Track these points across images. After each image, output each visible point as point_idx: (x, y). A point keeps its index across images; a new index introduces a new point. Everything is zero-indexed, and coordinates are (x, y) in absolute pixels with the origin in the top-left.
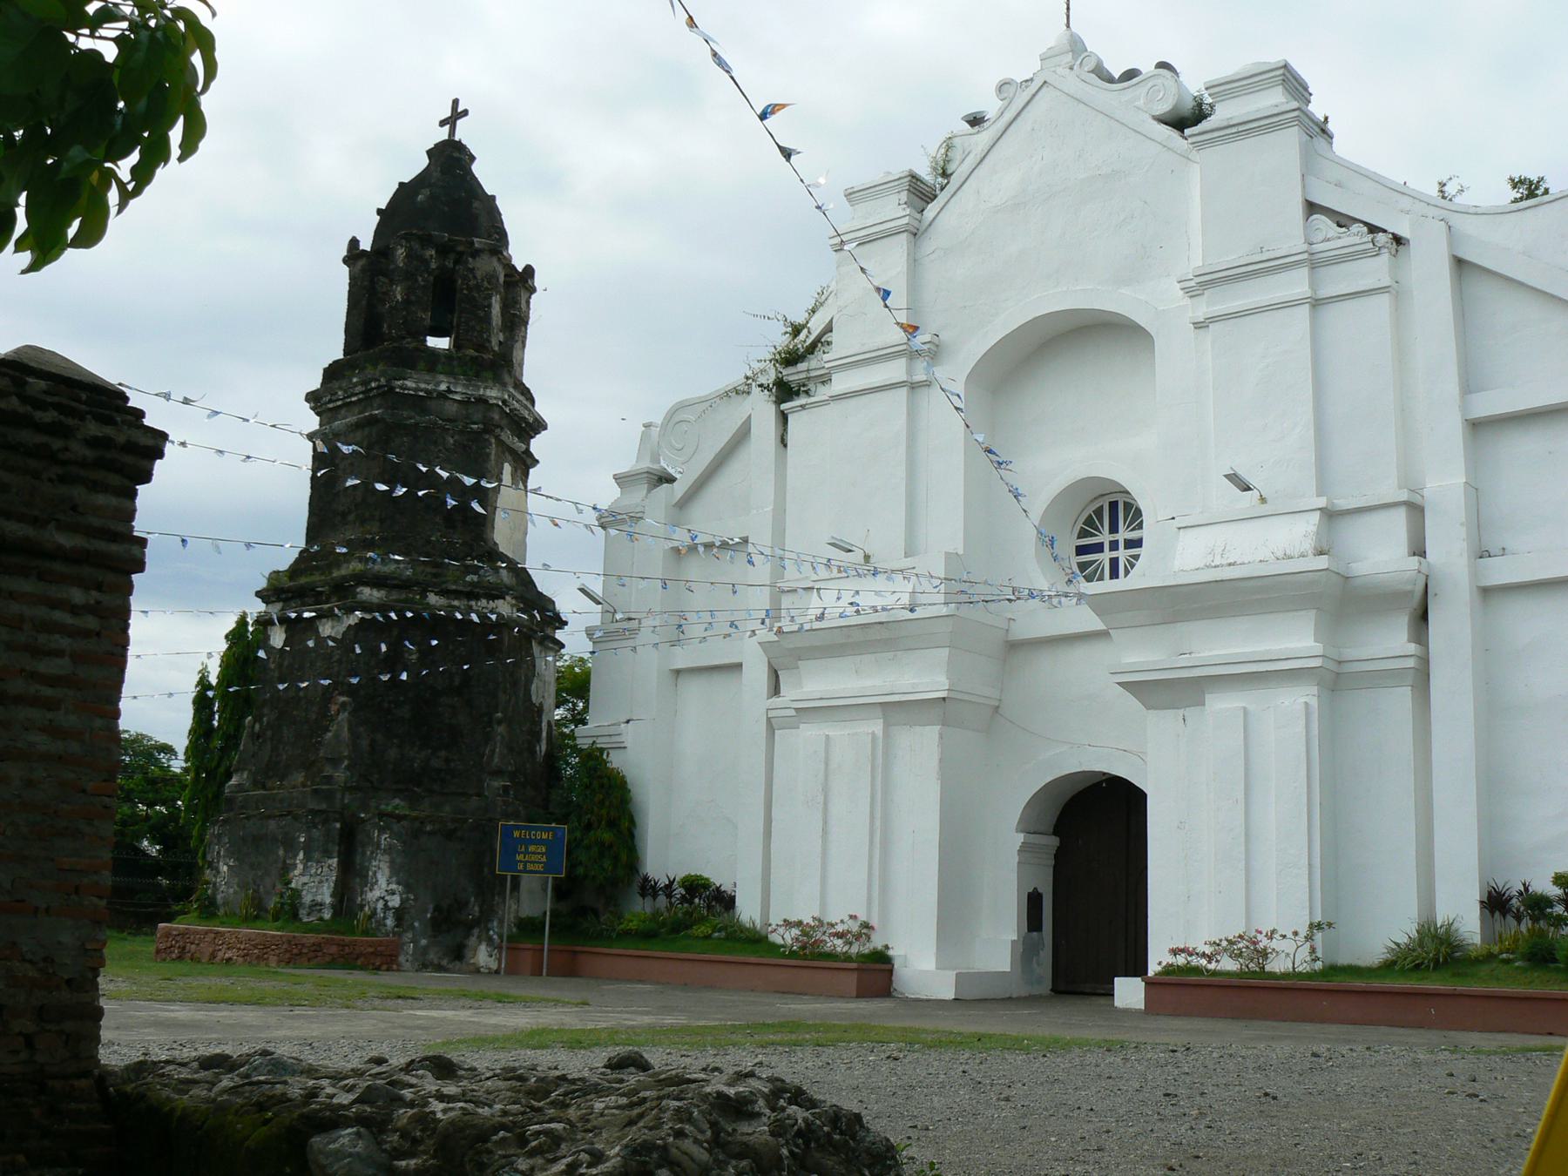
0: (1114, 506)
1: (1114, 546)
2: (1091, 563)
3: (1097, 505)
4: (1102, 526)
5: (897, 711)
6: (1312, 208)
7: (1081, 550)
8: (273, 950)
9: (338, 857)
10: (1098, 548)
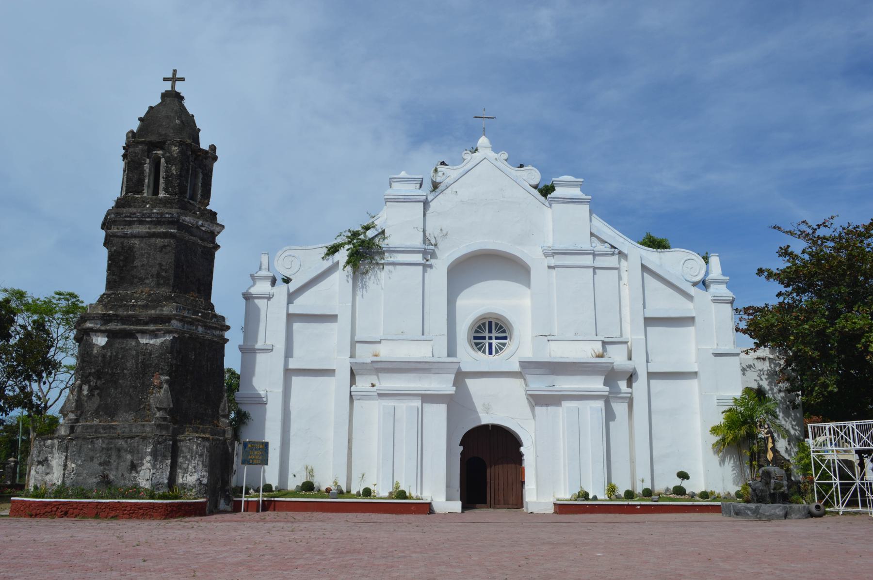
0: (490, 323)
1: (490, 338)
4: (485, 330)
5: (428, 398)
6: (592, 234)
7: (490, 353)
9: (171, 459)
10: (484, 338)
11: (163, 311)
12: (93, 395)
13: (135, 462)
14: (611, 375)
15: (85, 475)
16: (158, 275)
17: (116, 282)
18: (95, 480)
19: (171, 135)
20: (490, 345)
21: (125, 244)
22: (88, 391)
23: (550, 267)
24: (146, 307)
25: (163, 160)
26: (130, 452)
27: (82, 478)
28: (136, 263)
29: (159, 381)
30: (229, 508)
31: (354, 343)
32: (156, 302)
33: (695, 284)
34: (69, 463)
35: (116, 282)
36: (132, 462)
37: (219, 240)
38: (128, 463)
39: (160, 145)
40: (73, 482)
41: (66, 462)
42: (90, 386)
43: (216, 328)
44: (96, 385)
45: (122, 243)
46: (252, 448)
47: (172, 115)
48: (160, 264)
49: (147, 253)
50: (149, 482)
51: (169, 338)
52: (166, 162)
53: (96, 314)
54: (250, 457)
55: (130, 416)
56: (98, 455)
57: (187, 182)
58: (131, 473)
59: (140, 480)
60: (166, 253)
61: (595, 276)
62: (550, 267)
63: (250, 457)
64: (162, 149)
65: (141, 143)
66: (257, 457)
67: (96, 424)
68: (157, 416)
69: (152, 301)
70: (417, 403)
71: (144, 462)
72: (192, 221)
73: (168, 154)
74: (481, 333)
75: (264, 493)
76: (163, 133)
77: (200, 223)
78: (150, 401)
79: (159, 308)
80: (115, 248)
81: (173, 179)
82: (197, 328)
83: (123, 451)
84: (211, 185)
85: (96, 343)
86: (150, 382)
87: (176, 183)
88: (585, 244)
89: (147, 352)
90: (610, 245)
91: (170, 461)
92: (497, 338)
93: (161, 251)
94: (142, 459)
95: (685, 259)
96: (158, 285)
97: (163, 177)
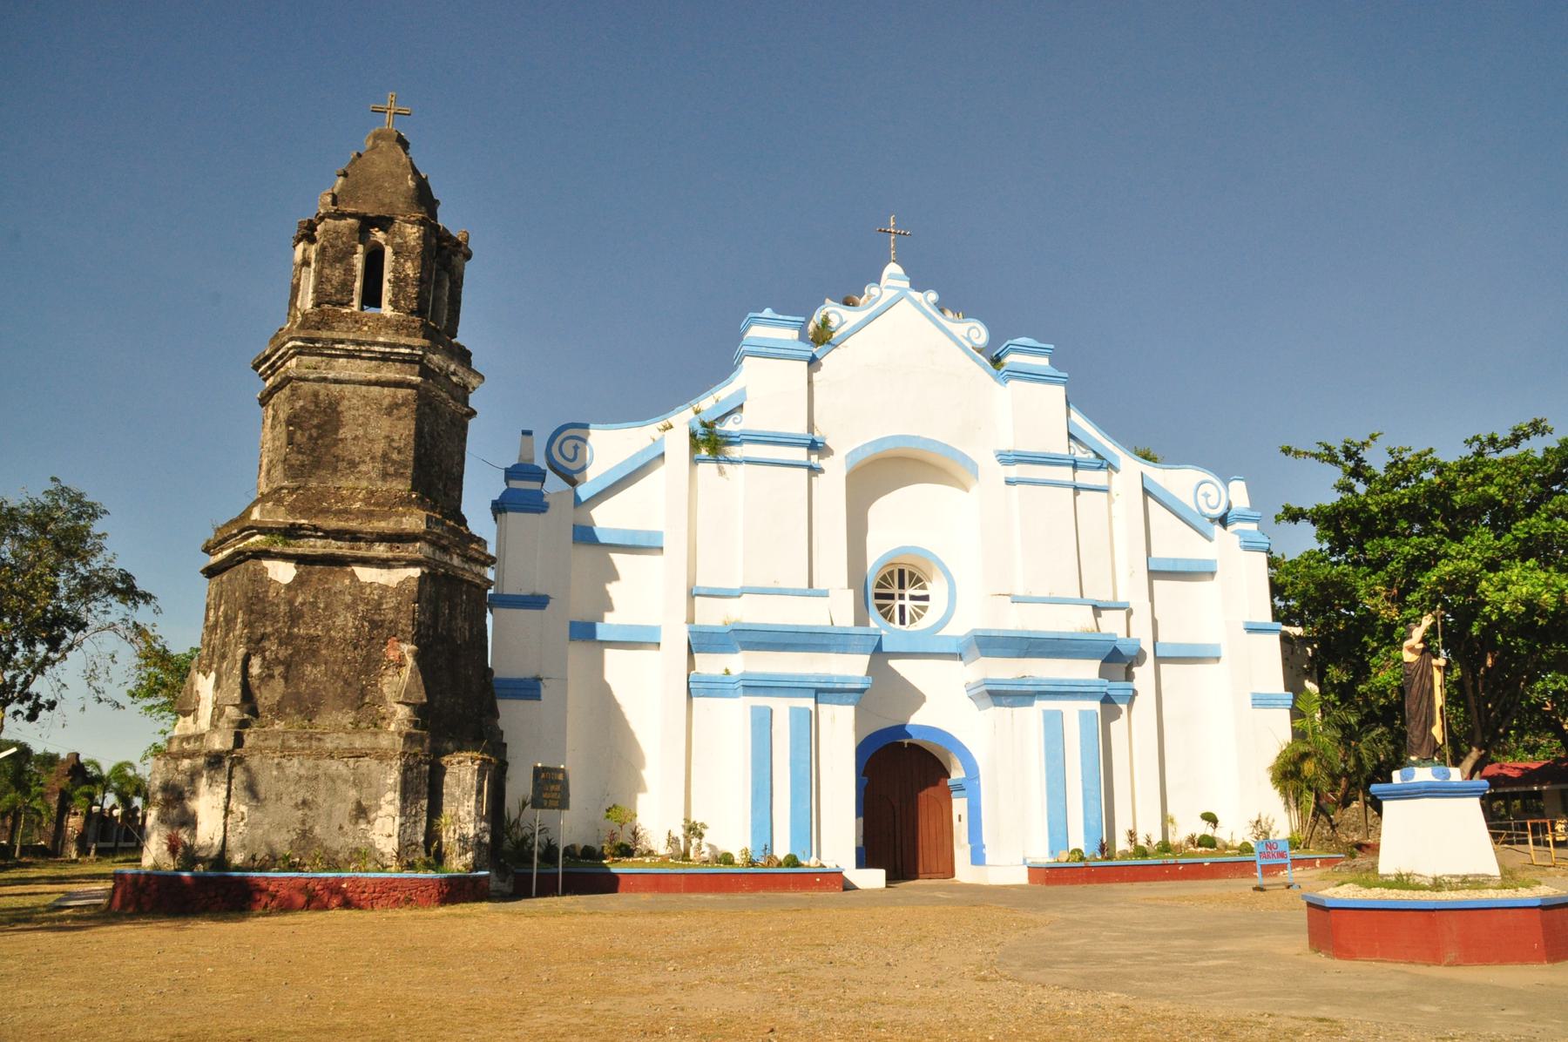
0: (901, 572)
2: (887, 605)
3: (890, 569)
5: (824, 692)
8: (422, 892)
10: (891, 597)
11: (401, 522)
12: (271, 676)
13: (364, 803)
14: (1119, 661)
15: (267, 827)
16: (385, 457)
17: (303, 466)
18: (287, 837)
19: (400, 206)
20: (902, 608)
21: (321, 398)
22: (260, 667)
23: (1008, 482)
24: (370, 515)
25: (388, 251)
26: (355, 784)
27: (260, 832)
28: (342, 433)
29: (398, 653)
30: (507, 888)
31: (692, 595)
32: (388, 505)
33: (1213, 520)
34: (233, 804)
35: (303, 466)
36: (359, 803)
37: (474, 401)
38: (351, 806)
39: (385, 223)
40: (243, 840)
41: (228, 803)
42: (264, 659)
43: (476, 561)
44: (277, 658)
45: (316, 395)
46: (546, 779)
47: (399, 171)
48: (388, 437)
49: (364, 416)
50: (395, 840)
51: (415, 572)
52: (396, 253)
53: (273, 522)
54: (545, 795)
55: (347, 718)
56: (292, 789)
57: (429, 292)
58: (357, 823)
59: (374, 837)
60: (400, 419)
61: (1078, 498)
62: (1008, 482)
63: (545, 795)
64: (385, 231)
65: (352, 215)
66: (554, 795)
67: (281, 729)
68: (400, 717)
69: (377, 504)
70: (809, 703)
71: (382, 802)
72: (442, 363)
73: (398, 240)
74: (910, 582)
75: (528, 871)
76: (387, 201)
77: (452, 367)
78: (382, 691)
79: (394, 519)
80: (301, 403)
81: (407, 285)
82: (451, 559)
83: (339, 782)
84: (460, 302)
85: (274, 578)
86: (380, 654)
87: (412, 291)
88: (1060, 447)
89: (373, 599)
90: (1094, 452)
91: (426, 801)
92: (913, 598)
93: (389, 414)
94: (378, 796)
95: (1199, 480)
96: (385, 476)
97: (389, 281)
